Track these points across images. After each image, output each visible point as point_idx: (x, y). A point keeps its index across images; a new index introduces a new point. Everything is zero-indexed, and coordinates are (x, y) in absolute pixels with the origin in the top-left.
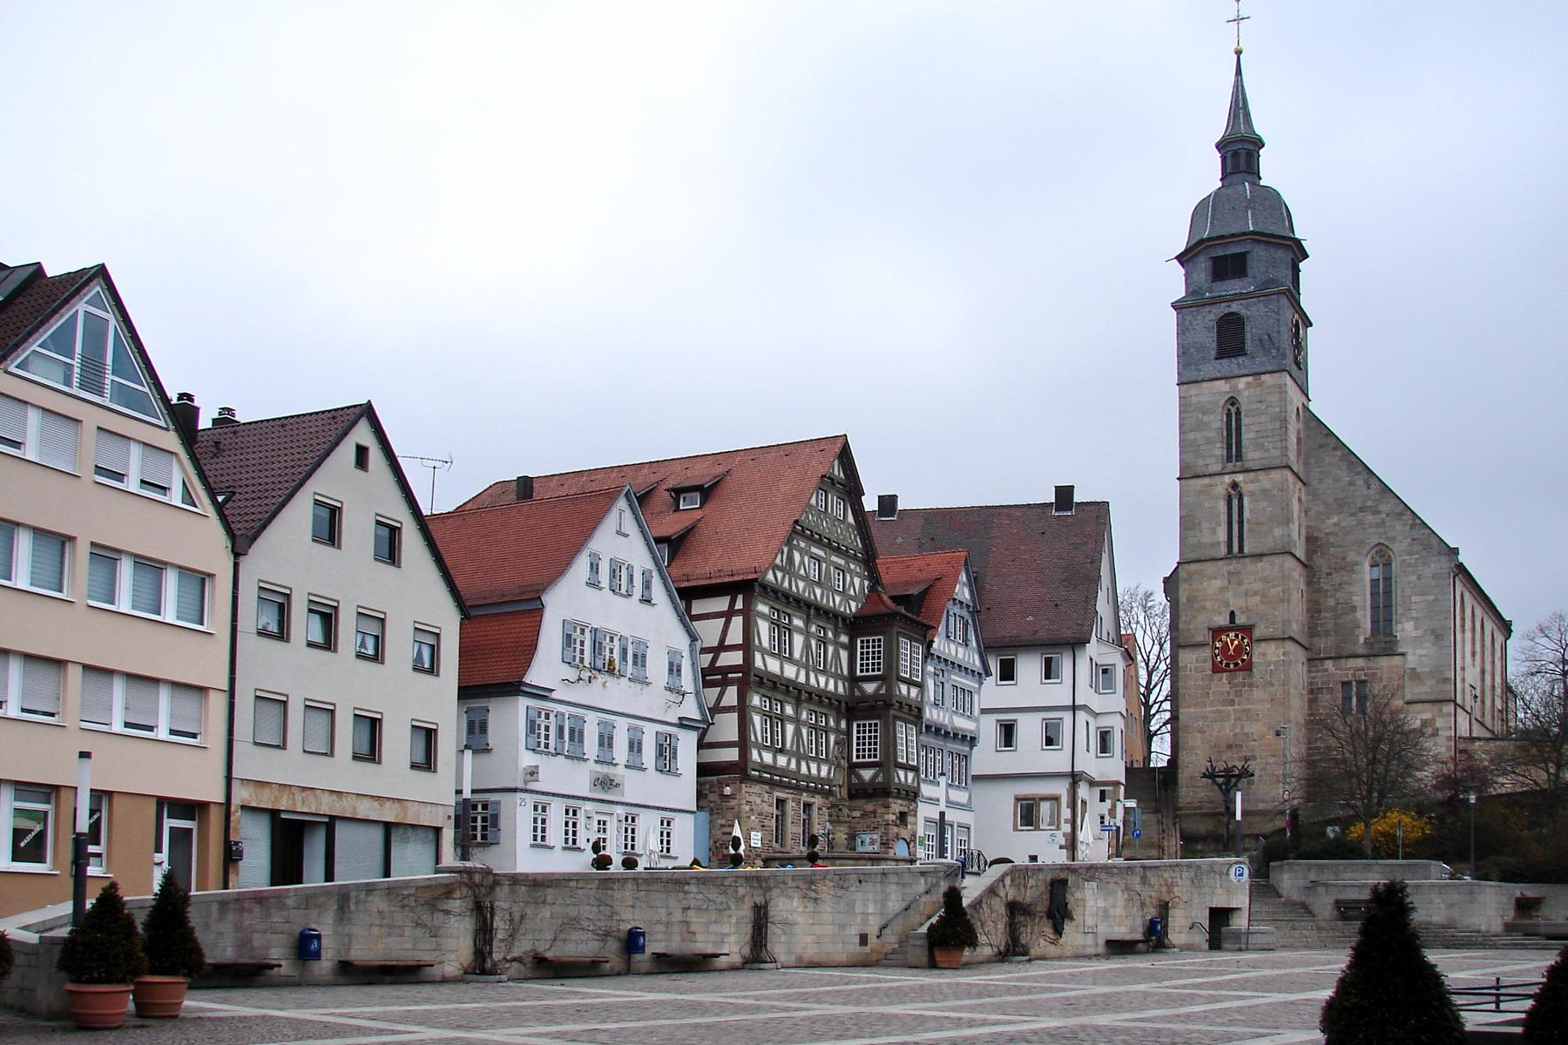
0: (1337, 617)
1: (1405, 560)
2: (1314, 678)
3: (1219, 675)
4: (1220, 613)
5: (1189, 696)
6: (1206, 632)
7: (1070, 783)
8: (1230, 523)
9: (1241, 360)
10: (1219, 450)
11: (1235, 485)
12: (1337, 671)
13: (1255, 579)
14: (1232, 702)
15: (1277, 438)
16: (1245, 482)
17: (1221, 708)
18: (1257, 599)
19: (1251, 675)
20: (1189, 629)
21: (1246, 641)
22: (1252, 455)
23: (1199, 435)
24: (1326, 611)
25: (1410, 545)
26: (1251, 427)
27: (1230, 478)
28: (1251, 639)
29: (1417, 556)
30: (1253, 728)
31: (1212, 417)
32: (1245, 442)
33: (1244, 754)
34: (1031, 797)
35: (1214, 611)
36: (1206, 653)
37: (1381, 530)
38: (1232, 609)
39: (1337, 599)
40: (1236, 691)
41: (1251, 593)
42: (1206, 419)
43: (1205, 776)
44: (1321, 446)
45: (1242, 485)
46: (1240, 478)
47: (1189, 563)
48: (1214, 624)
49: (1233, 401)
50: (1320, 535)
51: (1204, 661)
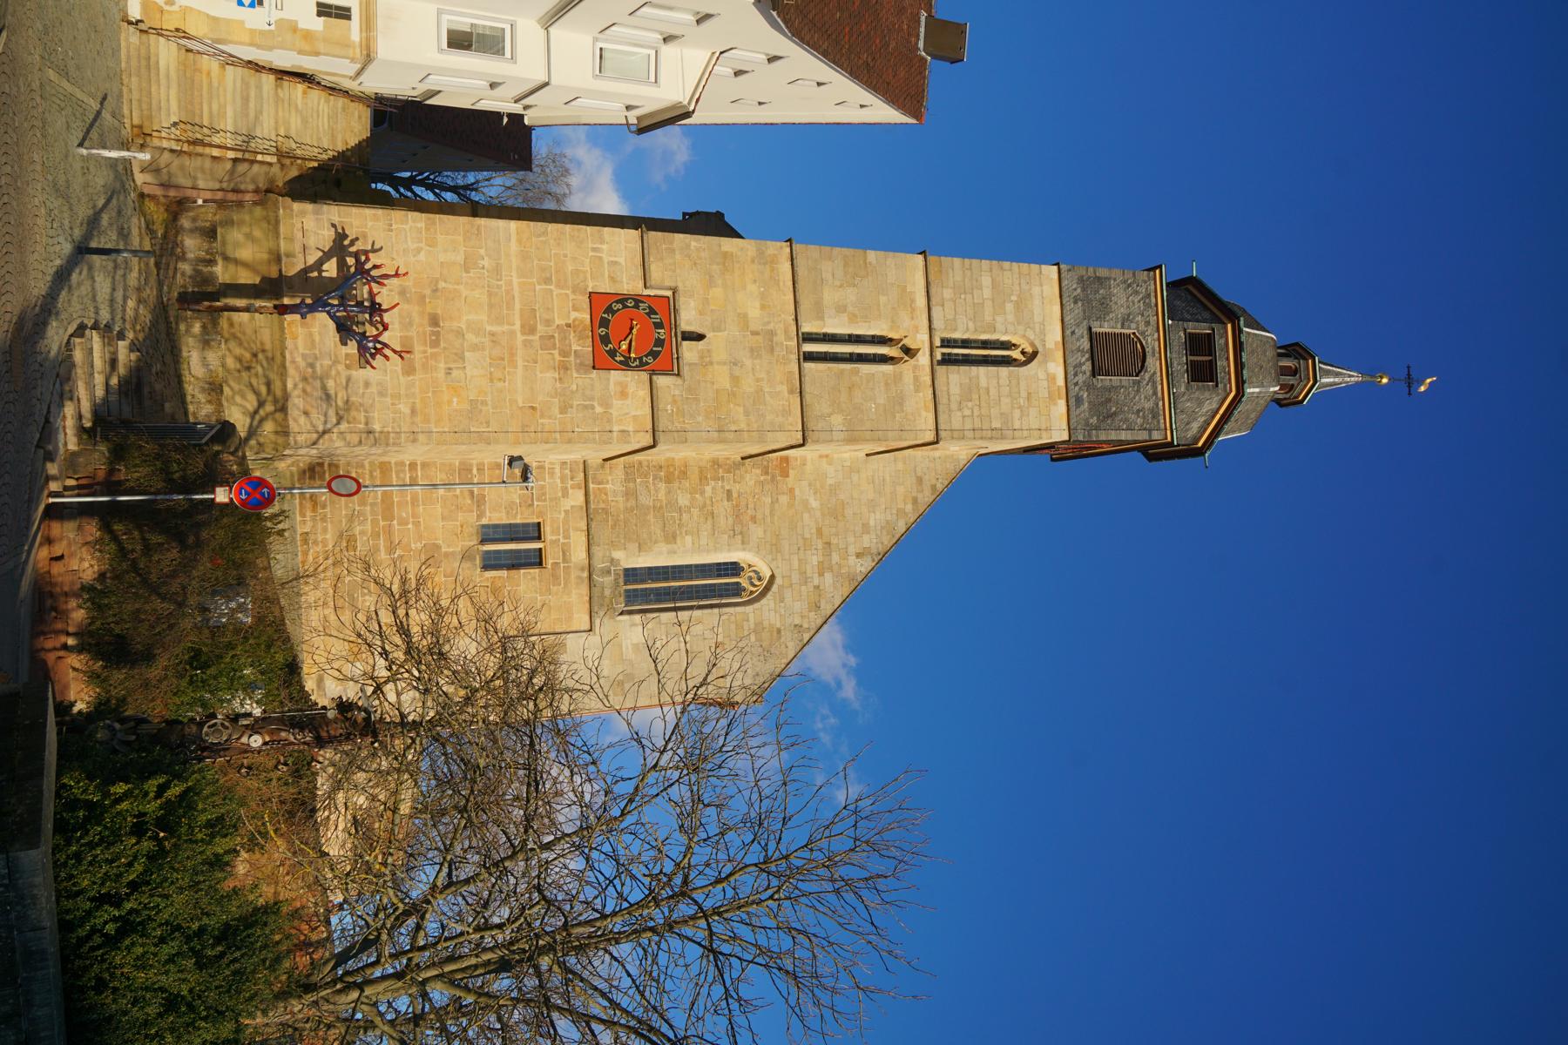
0: (658, 509)
1: (748, 621)
2: (552, 474)
3: (586, 306)
9: (1087, 367)
12: (563, 514)
13: (758, 380)
14: (529, 329)
16: (915, 367)
17: (518, 306)
18: (724, 382)
19: (581, 367)
22: (955, 378)
23: (987, 293)
26: (995, 381)
30: (474, 370)
32: (974, 370)
33: (417, 348)
35: (706, 301)
37: (795, 578)
38: (709, 335)
41: (737, 372)
42: (1009, 307)
44: (920, 480)
45: (912, 362)
46: (923, 359)
49: (1031, 357)
50: (791, 481)
51: (612, 279)
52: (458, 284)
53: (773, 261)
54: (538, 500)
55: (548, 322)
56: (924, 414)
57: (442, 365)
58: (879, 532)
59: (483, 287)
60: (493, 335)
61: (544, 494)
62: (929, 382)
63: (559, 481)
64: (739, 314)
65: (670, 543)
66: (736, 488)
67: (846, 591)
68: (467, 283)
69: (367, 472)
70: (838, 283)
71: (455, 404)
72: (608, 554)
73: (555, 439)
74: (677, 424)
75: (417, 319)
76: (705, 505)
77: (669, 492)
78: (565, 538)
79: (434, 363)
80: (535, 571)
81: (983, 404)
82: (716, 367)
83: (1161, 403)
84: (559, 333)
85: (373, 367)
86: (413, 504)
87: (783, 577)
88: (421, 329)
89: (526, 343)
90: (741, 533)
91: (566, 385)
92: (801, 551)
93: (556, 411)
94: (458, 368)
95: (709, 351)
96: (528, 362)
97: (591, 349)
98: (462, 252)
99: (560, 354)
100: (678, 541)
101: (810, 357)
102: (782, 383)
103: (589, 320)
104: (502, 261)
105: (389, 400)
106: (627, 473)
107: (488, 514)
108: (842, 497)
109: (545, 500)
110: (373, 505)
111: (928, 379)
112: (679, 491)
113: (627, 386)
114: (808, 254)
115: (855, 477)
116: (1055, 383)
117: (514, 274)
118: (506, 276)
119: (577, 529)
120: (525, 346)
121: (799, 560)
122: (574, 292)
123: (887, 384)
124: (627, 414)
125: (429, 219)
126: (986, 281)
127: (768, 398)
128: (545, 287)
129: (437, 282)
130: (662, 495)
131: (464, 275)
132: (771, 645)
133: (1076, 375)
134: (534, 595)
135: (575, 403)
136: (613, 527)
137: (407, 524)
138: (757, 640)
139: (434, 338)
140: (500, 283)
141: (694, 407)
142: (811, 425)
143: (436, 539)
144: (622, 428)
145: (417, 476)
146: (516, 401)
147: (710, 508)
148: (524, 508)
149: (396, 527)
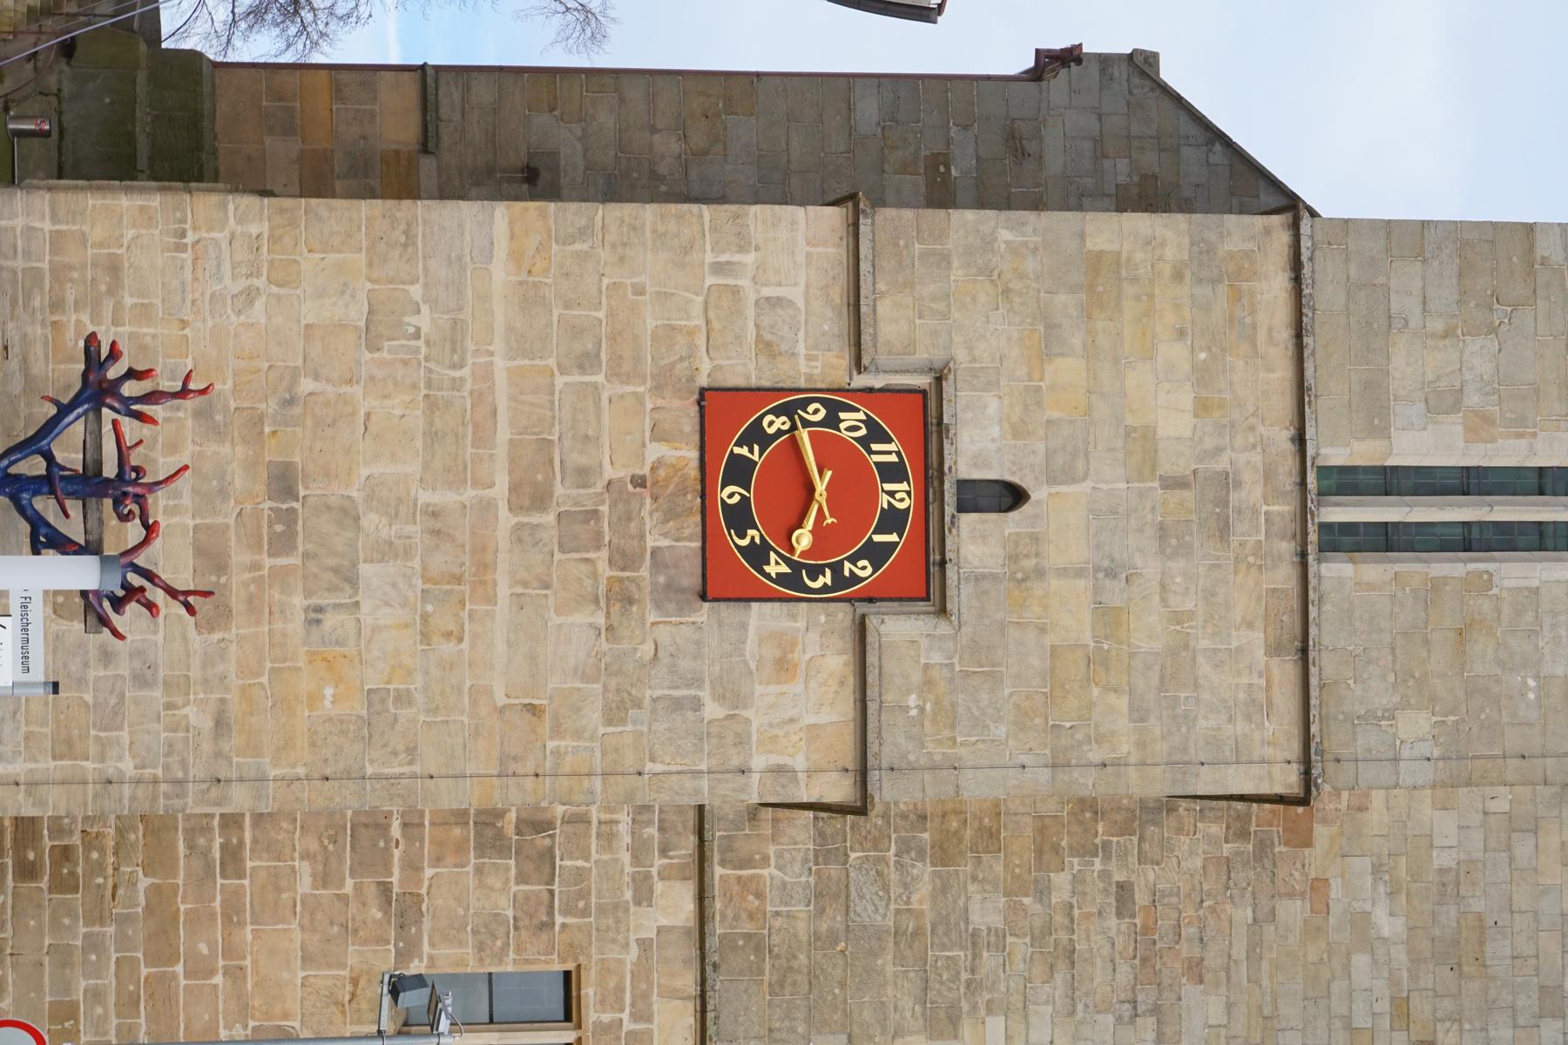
0: (907, 937)
2: (608, 838)
5: (582, 257)
6: (923, 355)
8: (1470, 482)
12: (634, 951)
13: (1178, 618)
17: (504, 434)
19: (667, 594)
20: (945, 259)
21: (864, 569)
24: (942, 889)
39: (998, 940)
41: (1115, 594)
43: (95, 358)
47: (1296, 265)
48: (964, 396)
50: (1317, 856)
51: (767, 348)
54: (566, 912)
57: (298, 601)
59: (415, 386)
60: (435, 515)
61: (584, 895)
63: (626, 858)
64: (1129, 431)
66: (1145, 879)
69: (112, 831)
70: (1438, 325)
71: (327, 703)
74: (930, 747)
75: (239, 481)
76: (1048, 929)
77: (944, 890)
78: (635, 1017)
84: (613, 504)
86: (227, 918)
88: (248, 507)
89: (520, 535)
90: (1156, 1010)
91: (625, 646)
93: (593, 717)
94: (336, 606)
95: (1035, 539)
96: (525, 584)
97: (697, 544)
100: (966, 1030)
101: (1343, 539)
102: (1250, 625)
103: (695, 464)
105: (158, 693)
106: (821, 834)
107: (426, 948)
108: (1478, 905)
109: (585, 913)
112: (971, 888)
113: (793, 645)
115: (1524, 849)
117: (498, 346)
119: (671, 994)
122: (658, 389)
124: (792, 720)
125: (281, 211)
127: (1205, 668)
128: (576, 378)
129: (294, 380)
130: (921, 897)
131: (367, 356)
136: (777, 988)
137: (212, 973)
139: (279, 528)
140: (457, 374)
141: (985, 698)
142: (1332, 738)
143: (286, 1016)
144: (776, 759)
145: (241, 843)
146: (489, 692)
147: (1063, 936)
149: (183, 982)
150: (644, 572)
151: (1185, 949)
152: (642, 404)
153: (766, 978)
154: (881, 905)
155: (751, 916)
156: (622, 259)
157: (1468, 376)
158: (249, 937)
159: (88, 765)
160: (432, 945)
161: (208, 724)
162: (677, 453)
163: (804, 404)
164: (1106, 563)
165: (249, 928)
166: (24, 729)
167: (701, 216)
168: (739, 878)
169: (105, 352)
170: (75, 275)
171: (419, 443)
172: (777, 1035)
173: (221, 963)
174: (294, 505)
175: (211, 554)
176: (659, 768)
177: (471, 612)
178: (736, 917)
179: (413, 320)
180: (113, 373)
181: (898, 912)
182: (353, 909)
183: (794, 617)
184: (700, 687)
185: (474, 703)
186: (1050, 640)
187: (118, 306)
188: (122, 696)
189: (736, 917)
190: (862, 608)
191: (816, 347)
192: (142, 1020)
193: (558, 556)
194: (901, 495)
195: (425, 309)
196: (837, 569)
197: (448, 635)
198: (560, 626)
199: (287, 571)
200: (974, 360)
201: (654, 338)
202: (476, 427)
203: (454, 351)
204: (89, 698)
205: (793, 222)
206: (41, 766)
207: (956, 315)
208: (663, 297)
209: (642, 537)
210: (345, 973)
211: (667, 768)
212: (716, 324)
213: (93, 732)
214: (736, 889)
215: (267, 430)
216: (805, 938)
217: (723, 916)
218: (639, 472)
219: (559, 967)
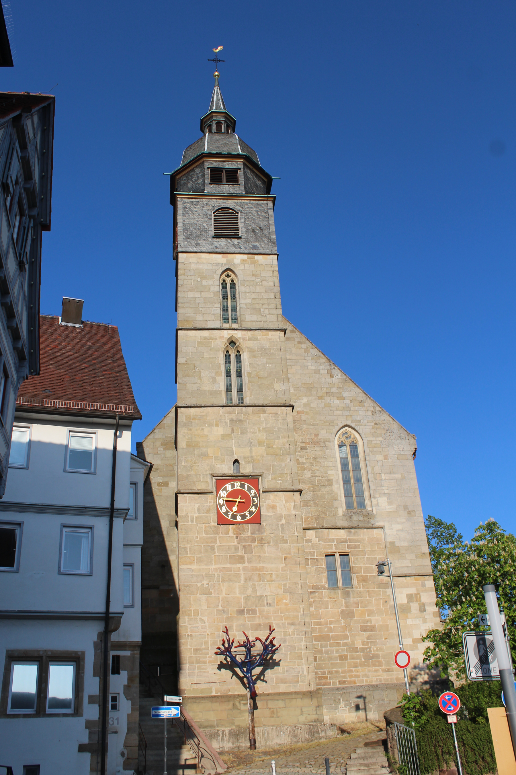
1: (371, 441)
3: (225, 527)
4: (223, 461)
7: (99, 634)
9: (236, 241)
10: (217, 309)
11: (232, 342)
12: (320, 542)
13: (259, 430)
14: (241, 560)
15: (272, 306)
16: (244, 339)
17: (228, 565)
18: (261, 450)
19: (260, 531)
20: (188, 475)
23: (197, 295)
25: (373, 428)
27: (229, 334)
28: (258, 490)
29: (381, 439)
31: (211, 282)
34: (36, 654)
36: (209, 501)
37: (347, 413)
40: (244, 546)
42: (204, 283)
45: (241, 341)
46: (238, 335)
51: (208, 511)
52: (219, 598)
53: (189, 418)
54: (314, 556)
55: (237, 549)
56: (270, 336)
57: (266, 608)
58: (319, 364)
59: (219, 584)
60: (246, 580)
61: (310, 552)
62: (252, 332)
65: (332, 483)
67: (352, 385)
68: (218, 594)
70: (199, 381)
71: (287, 601)
72: (341, 518)
73: (301, 546)
77: (304, 482)
78: (334, 542)
79: (265, 613)
80: (352, 558)
81: (261, 302)
82: (253, 454)
83: (252, 201)
85: (280, 646)
86: (320, 625)
87: (347, 420)
89: (249, 561)
90: (324, 442)
92: (332, 409)
93: (286, 546)
94: (266, 600)
96: (260, 560)
98: (200, 596)
99: (254, 543)
100: (331, 478)
102: (260, 417)
104: (204, 574)
105: (287, 637)
107: (323, 584)
109: (314, 552)
110: (322, 646)
111: (250, 333)
112: (304, 477)
114: (183, 398)
116: (246, 260)
117: (210, 567)
118: (212, 572)
120: (251, 562)
121: (337, 410)
123: (255, 356)
124: (284, 506)
126: (190, 295)
127: (268, 425)
131: (213, 595)
132: (384, 429)
133: (240, 248)
134: (365, 559)
135: (281, 535)
137: (331, 627)
138: (381, 437)
139: (251, 613)
143: (339, 612)
146: (282, 568)
148: (319, 564)
149: (333, 633)
150: (256, 536)
151: (312, 437)
152: (221, 537)
153: (324, 516)
154: (308, 494)
155: (312, 519)
156: (191, 541)
157: (209, 376)
158: (323, 620)
159: (303, 652)
160: (322, 583)
161: (293, 627)
162: (231, 529)
163: (220, 504)
164: (249, 444)
165: (321, 620)
166: (296, 666)
167: (181, 525)
168: (305, 522)
169: (219, 651)
170: (198, 658)
171: (231, 583)
172: (335, 514)
173: (329, 626)
174: (245, 610)
175: (257, 627)
176: (296, 532)
177: (266, 572)
178: (313, 522)
179: (205, 585)
180: (223, 648)
181: (309, 491)
182: (316, 599)
183: (263, 505)
184: (279, 524)
185: (285, 571)
186: (265, 455)
187: (204, 649)
188: (288, 645)
189: (313, 522)
190: (261, 491)
191: (208, 501)
192: (341, 641)
193: (253, 554)
194: (237, 485)
195: (203, 583)
196: (253, 497)
197: (271, 576)
198: (268, 553)
199: (259, 610)
200: (209, 470)
201: (207, 534)
202: (227, 571)
203: (211, 576)
204: (289, 653)
205: (182, 506)
206: (304, 662)
207: (200, 473)
208: (198, 533)
209: (249, 536)
210: (329, 600)
211: (296, 531)
212: (204, 522)
213: (296, 651)
214: (307, 522)
215: (230, 616)
216: (316, 509)
217: (313, 525)
218: (235, 537)
219: (324, 558)
